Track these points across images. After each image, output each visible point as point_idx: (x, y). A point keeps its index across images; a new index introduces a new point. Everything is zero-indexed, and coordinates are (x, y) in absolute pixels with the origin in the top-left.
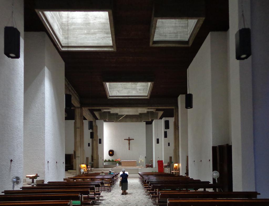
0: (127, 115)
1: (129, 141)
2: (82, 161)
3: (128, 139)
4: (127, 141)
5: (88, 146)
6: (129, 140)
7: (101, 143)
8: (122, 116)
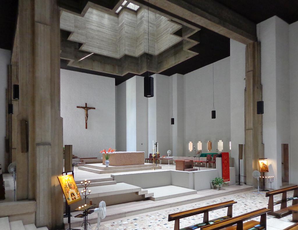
0: (95, 55)
1: (87, 111)
2: (16, 197)
3: (84, 106)
4: (83, 111)
5: (85, 128)
6: (86, 108)
7: (215, 118)
8: (89, 53)
